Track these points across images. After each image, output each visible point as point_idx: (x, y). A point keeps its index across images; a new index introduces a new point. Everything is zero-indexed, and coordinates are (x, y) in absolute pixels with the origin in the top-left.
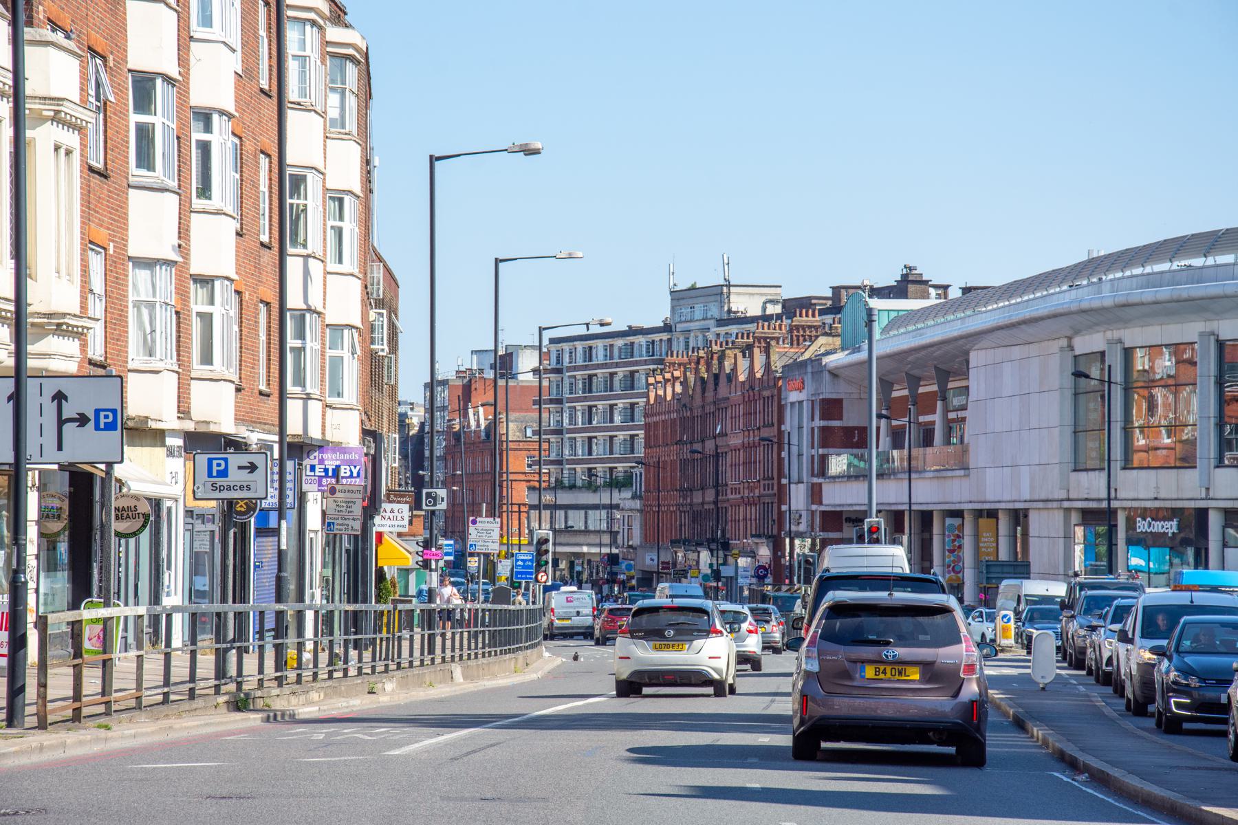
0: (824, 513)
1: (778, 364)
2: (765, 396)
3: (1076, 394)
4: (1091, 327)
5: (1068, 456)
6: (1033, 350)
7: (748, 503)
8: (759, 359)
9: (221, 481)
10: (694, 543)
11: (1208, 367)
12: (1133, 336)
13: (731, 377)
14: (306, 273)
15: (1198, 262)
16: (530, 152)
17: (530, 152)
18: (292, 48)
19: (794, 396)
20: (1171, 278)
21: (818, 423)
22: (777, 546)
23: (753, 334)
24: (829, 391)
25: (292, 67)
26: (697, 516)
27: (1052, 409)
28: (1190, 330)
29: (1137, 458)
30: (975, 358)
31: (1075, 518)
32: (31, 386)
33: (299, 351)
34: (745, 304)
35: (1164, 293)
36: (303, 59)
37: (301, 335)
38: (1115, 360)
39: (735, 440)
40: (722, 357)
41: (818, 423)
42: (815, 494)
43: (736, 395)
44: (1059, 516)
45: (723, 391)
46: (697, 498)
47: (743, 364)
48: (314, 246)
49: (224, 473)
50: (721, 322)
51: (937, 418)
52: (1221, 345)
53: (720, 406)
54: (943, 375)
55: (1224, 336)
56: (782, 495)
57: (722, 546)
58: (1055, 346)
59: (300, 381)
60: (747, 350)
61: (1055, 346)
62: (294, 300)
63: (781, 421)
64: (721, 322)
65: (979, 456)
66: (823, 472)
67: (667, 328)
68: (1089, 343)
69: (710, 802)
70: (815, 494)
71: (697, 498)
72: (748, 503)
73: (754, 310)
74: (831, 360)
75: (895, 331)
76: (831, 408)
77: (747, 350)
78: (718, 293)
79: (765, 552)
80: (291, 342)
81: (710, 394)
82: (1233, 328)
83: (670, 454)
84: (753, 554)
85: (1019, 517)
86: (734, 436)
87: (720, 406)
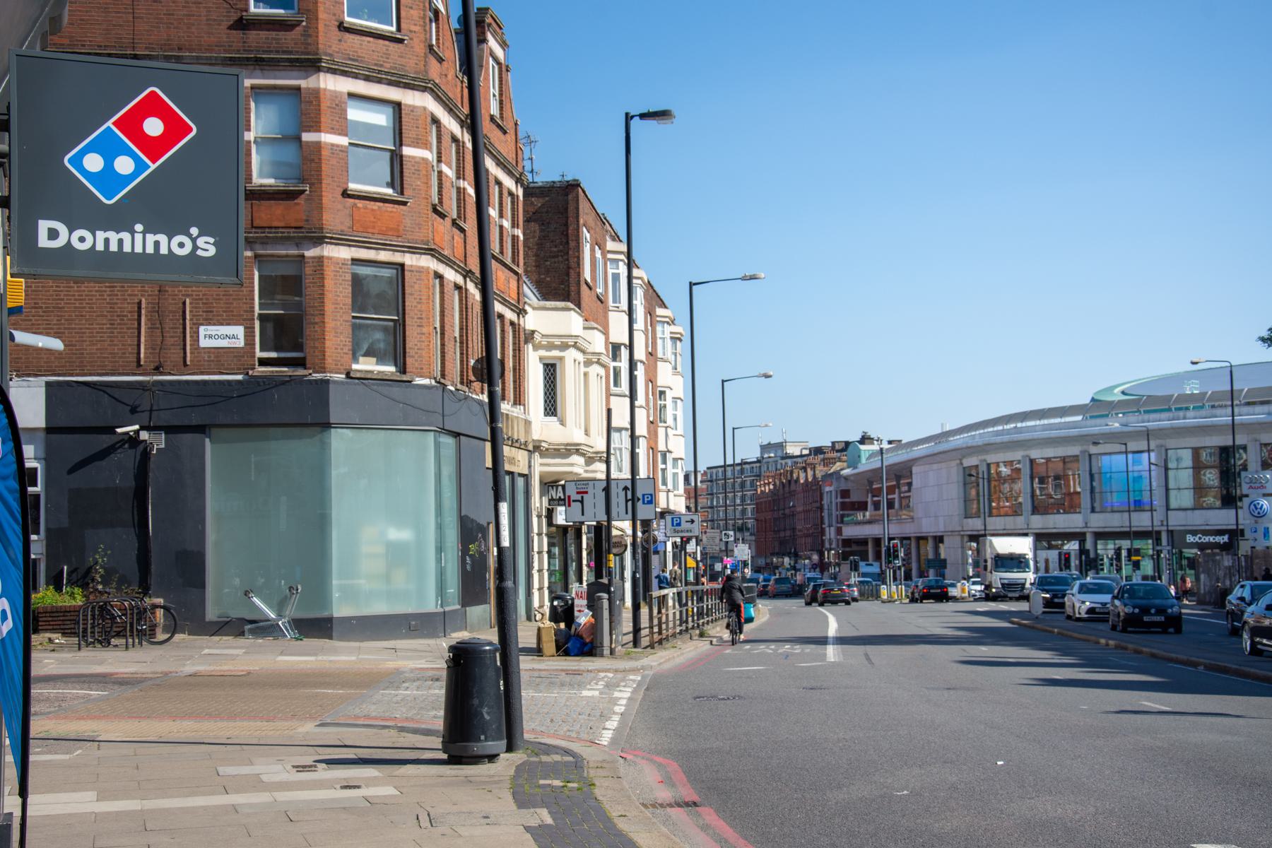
0: (844, 540)
1: (819, 475)
2: (814, 488)
3: (965, 484)
4: (970, 455)
5: (962, 512)
6: (943, 465)
7: (807, 536)
8: (810, 473)
9: (678, 528)
10: (782, 554)
11: (1026, 472)
12: (991, 458)
13: (798, 480)
14: (667, 435)
15: (1019, 425)
16: (767, 376)
17: (767, 376)
18: (659, 335)
19: (827, 489)
20: (998, 433)
21: (839, 500)
22: (821, 555)
23: (804, 462)
24: (844, 486)
25: (659, 342)
26: (782, 542)
27: (953, 491)
28: (1017, 455)
29: (994, 511)
30: (915, 470)
31: (966, 539)
32: (613, 484)
33: (664, 470)
34: (793, 450)
35: (1006, 438)
36: (663, 339)
37: (664, 462)
38: (983, 468)
39: (800, 509)
40: (792, 472)
41: (839, 500)
42: (839, 531)
43: (799, 489)
44: (958, 538)
45: (793, 487)
46: (782, 534)
47: (802, 475)
48: (670, 421)
49: (679, 524)
50: (783, 458)
51: (896, 496)
52: (1032, 461)
53: (792, 494)
54: (898, 478)
55: (1033, 457)
56: (823, 532)
57: (796, 556)
58: (954, 463)
59: (665, 483)
60: (805, 469)
61: (954, 463)
62: (661, 447)
63: (822, 499)
64: (783, 458)
65: (918, 512)
66: (842, 522)
67: (759, 461)
68: (968, 462)
69: (1052, 688)
70: (839, 531)
71: (782, 534)
72: (807, 536)
73: (798, 453)
74: (845, 472)
75: (867, 458)
76: (845, 493)
77: (805, 469)
78: (781, 446)
79: (815, 557)
80: (661, 466)
81: (787, 489)
82: (1266, 438)
83: (769, 516)
84: (810, 558)
85: (939, 540)
86: (797, 504)
87: (792, 494)
